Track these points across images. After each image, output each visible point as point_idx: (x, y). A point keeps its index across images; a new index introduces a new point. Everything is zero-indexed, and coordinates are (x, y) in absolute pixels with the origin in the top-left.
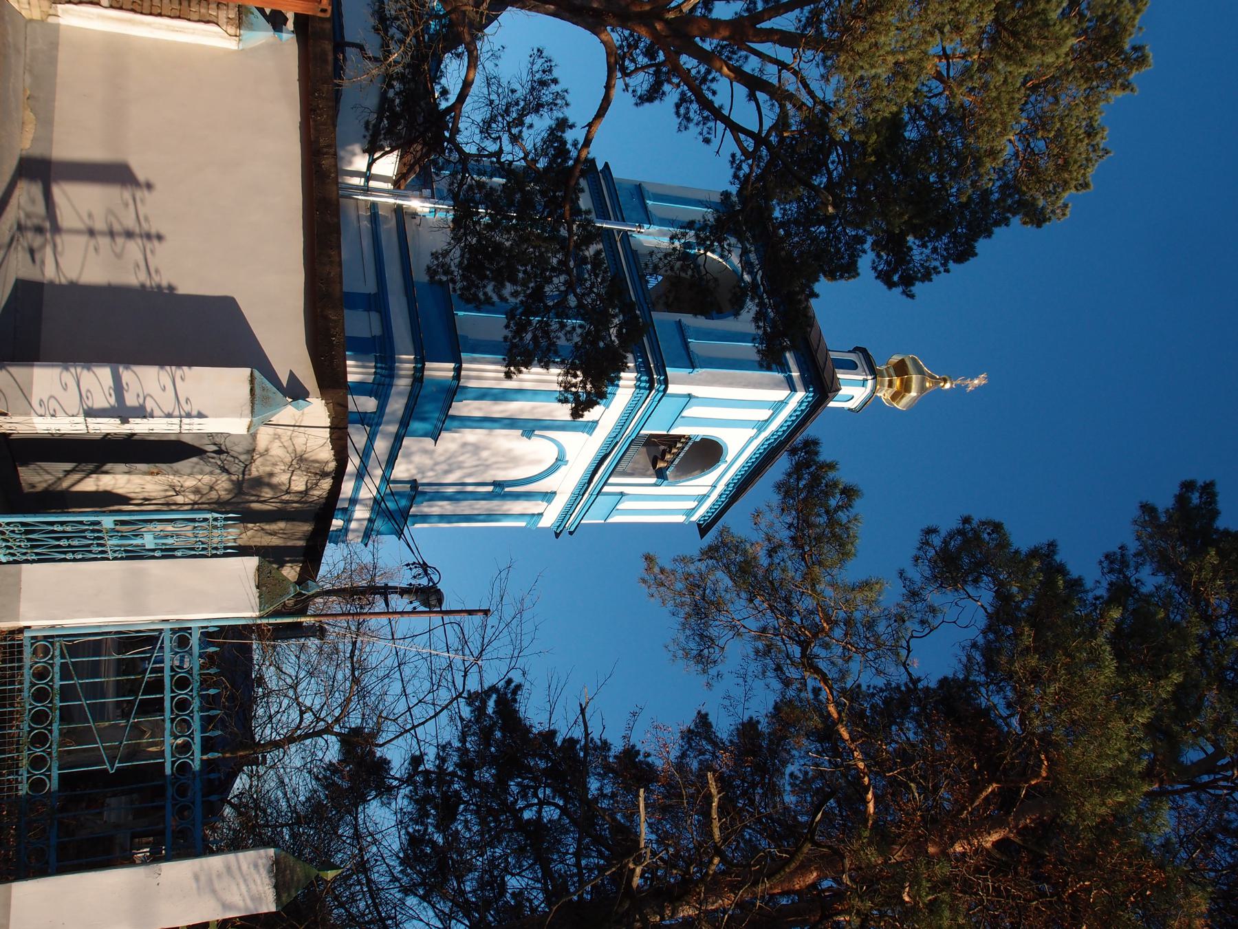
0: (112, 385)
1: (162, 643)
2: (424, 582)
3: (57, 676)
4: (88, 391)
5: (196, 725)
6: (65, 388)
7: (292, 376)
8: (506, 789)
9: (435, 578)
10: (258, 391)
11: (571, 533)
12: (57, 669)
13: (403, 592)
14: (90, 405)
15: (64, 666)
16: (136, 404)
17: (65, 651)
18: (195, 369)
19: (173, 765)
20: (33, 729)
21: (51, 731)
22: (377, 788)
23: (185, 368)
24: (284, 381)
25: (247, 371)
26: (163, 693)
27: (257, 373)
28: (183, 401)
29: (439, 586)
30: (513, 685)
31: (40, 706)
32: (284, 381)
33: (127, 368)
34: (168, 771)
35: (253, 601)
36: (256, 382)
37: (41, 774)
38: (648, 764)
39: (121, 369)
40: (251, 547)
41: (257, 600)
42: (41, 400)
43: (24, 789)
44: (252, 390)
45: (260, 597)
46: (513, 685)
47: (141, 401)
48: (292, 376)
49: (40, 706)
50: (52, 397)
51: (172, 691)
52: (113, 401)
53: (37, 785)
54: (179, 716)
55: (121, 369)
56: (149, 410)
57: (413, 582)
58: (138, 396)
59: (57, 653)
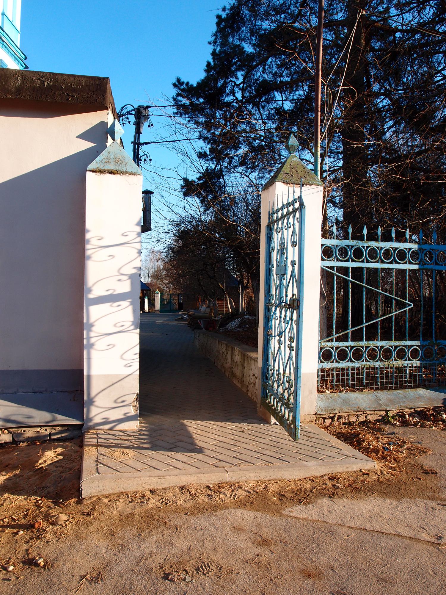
0: (109, 304)
1: (327, 267)
2: (132, 118)
3: (346, 344)
4: (115, 325)
5: (387, 245)
6: (111, 346)
7: (83, 136)
8: (229, 104)
9: (130, 108)
10: (112, 167)
11: (26, 58)
12: (341, 344)
13: (138, 132)
14: (130, 323)
15: (338, 339)
16: (128, 282)
17: (329, 338)
18: (88, 225)
19: (412, 263)
20: (350, 359)
21: (382, 347)
22: (219, 178)
23: (88, 236)
24: (87, 145)
25: (90, 175)
26: (363, 268)
27: (91, 166)
28: (125, 240)
29: (136, 107)
30: (177, 83)
31: (365, 355)
32: (87, 145)
33: (90, 291)
34: (416, 267)
35: (313, 191)
36: (102, 167)
37: (408, 352)
38: (231, 9)
39: (91, 296)
40: (271, 185)
41: (313, 187)
42: (125, 366)
43: (416, 363)
44: (111, 173)
45: (311, 185)
46: (177, 83)
47: (126, 278)
48: (83, 136)
49: (365, 355)
50: (121, 357)
51: (363, 261)
52: (125, 304)
53: (415, 354)
54: (380, 257)
55: (91, 296)
56: (134, 271)
57: (132, 123)
58: (119, 280)
59: (329, 344)
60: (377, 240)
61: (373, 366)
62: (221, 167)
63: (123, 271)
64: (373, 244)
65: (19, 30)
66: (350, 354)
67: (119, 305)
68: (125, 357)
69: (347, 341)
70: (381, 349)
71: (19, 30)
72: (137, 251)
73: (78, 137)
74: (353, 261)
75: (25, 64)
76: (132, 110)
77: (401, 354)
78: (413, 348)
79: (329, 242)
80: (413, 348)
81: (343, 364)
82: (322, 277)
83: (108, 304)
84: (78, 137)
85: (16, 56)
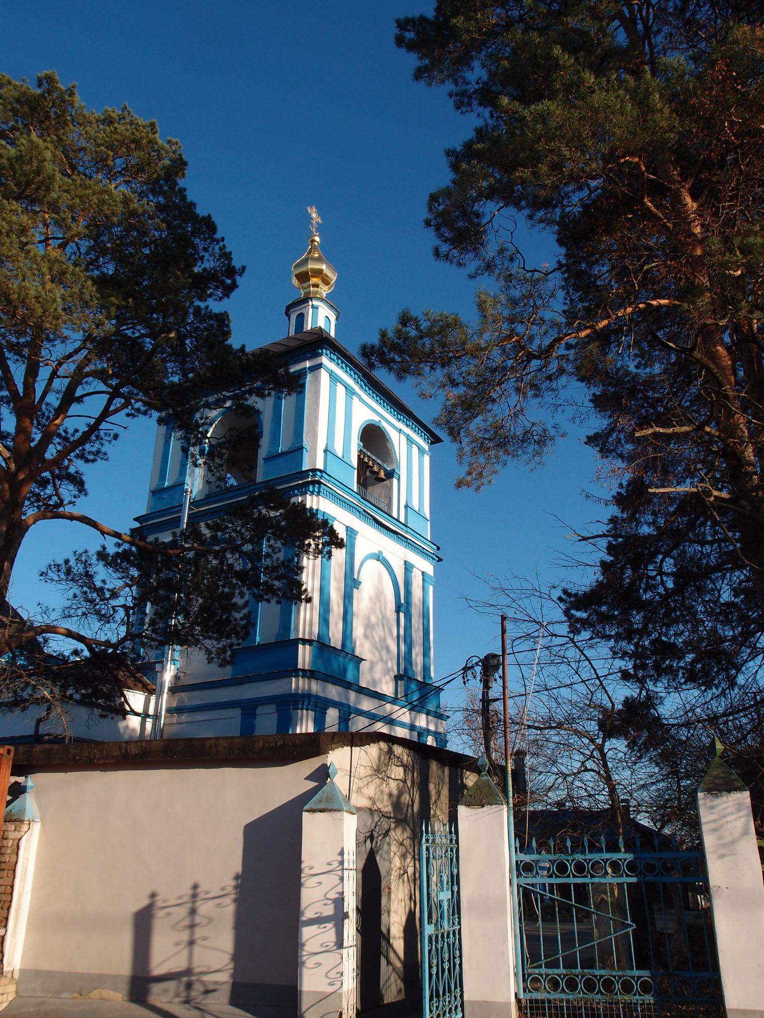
1: (528, 884)
4: (321, 945)
5: (596, 857)
6: (319, 964)
7: (309, 778)
8: (649, 602)
9: (475, 660)
10: (322, 806)
11: (438, 548)
12: (550, 971)
13: (487, 687)
15: (548, 966)
16: (332, 906)
21: (601, 976)
23: (303, 866)
28: (330, 868)
29: (482, 657)
30: (563, 596)
31: (581, 986)
33: (303, 914)
34: (634, 880)
36: (314, 807)
37: (637, 985)
39: (304, 919)
41: (485, 808)
43: (649, 999)
44: (321, 811)
45: (491, 805)
47: (330, 902)
48: (309, 778)
49: (581, 986)
50: (326, 976)
52: (330, 925)
53: (645, 988)
55: (304, 919)
56: (337, 896)
57: (479, 678)
58: (325, 904)
59: (537, 971)
60: (600, 850)
61: (629, 1001)
62: (647, 693)
63: (328, 896)
64: (579, 857)
65: (428, 517)
66: (562, 984)
67: (325, 927)
68: (330, 975)
69: (558, 967)
70: (600, 978)
71: (428, 517)
72: (338, 878)
73: (305, 779)
74: (557, 876)
75: (437, 557)
76: (479, 662)
77: (627, 987)
78: (642, 979)
79: (527, 858)
80: (642, 979)
81: (555, 996)
82: (357, 914)
83: (316, 926)
84: (305, 779)
85: (425, 551)
